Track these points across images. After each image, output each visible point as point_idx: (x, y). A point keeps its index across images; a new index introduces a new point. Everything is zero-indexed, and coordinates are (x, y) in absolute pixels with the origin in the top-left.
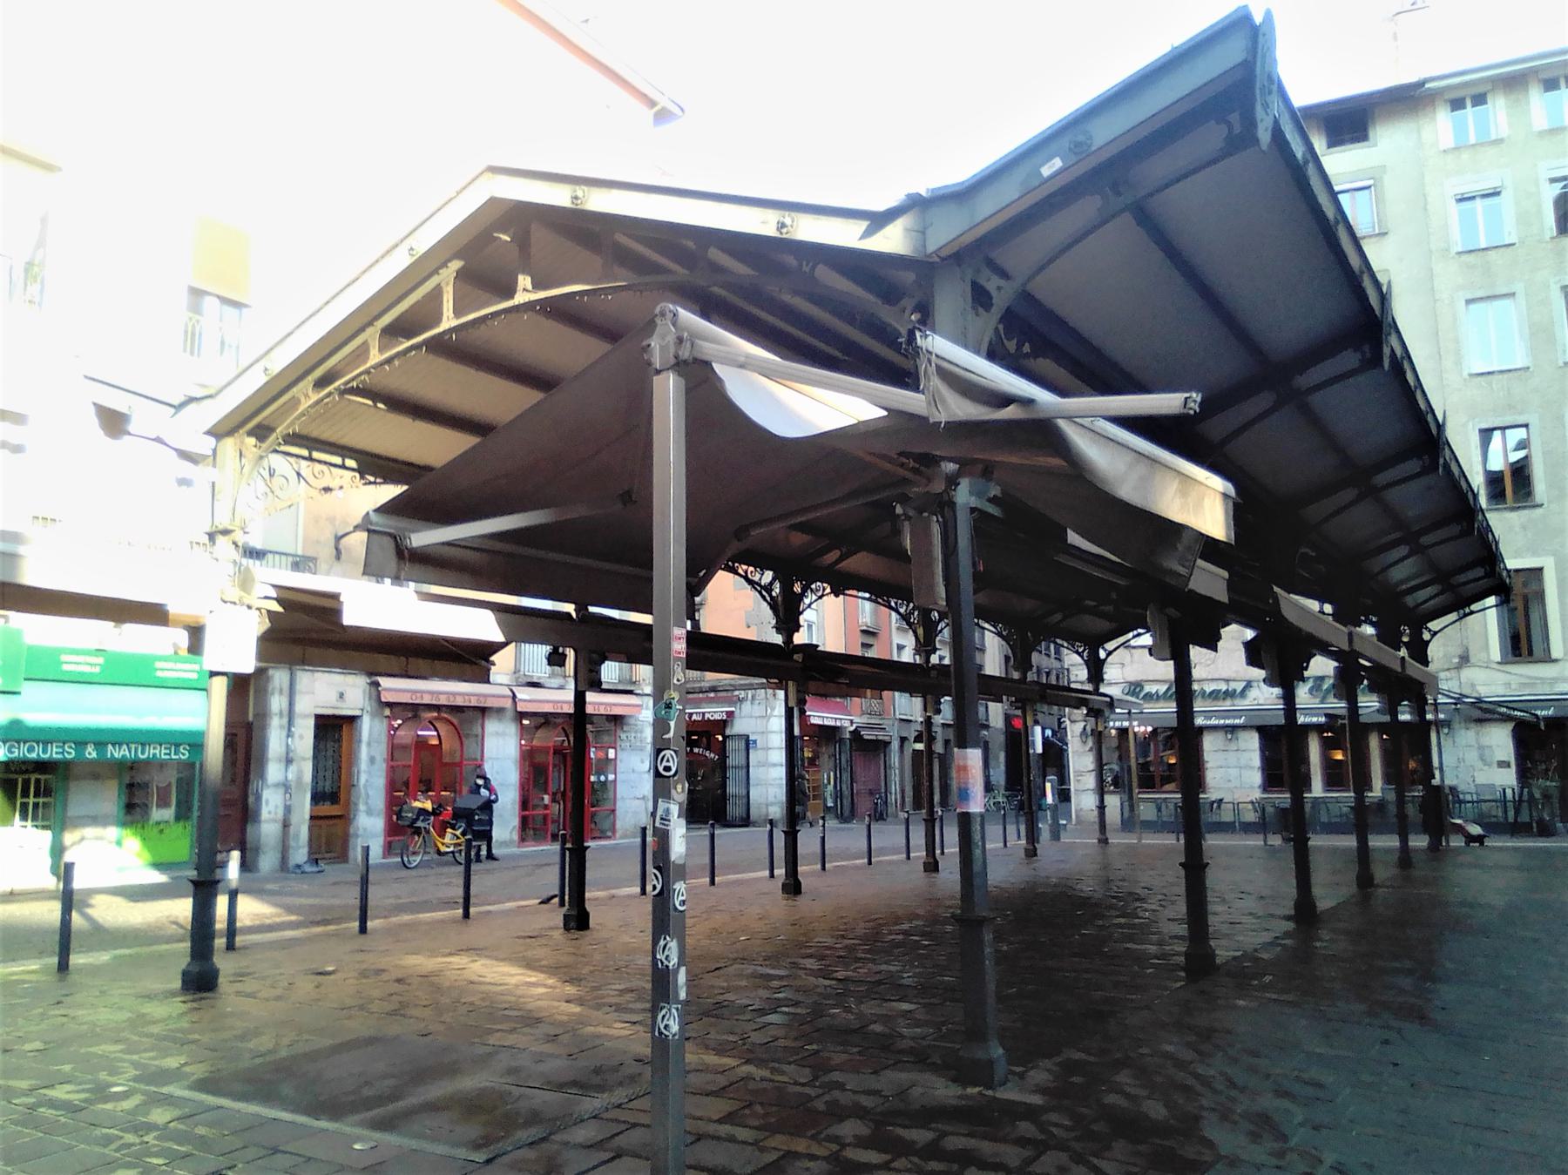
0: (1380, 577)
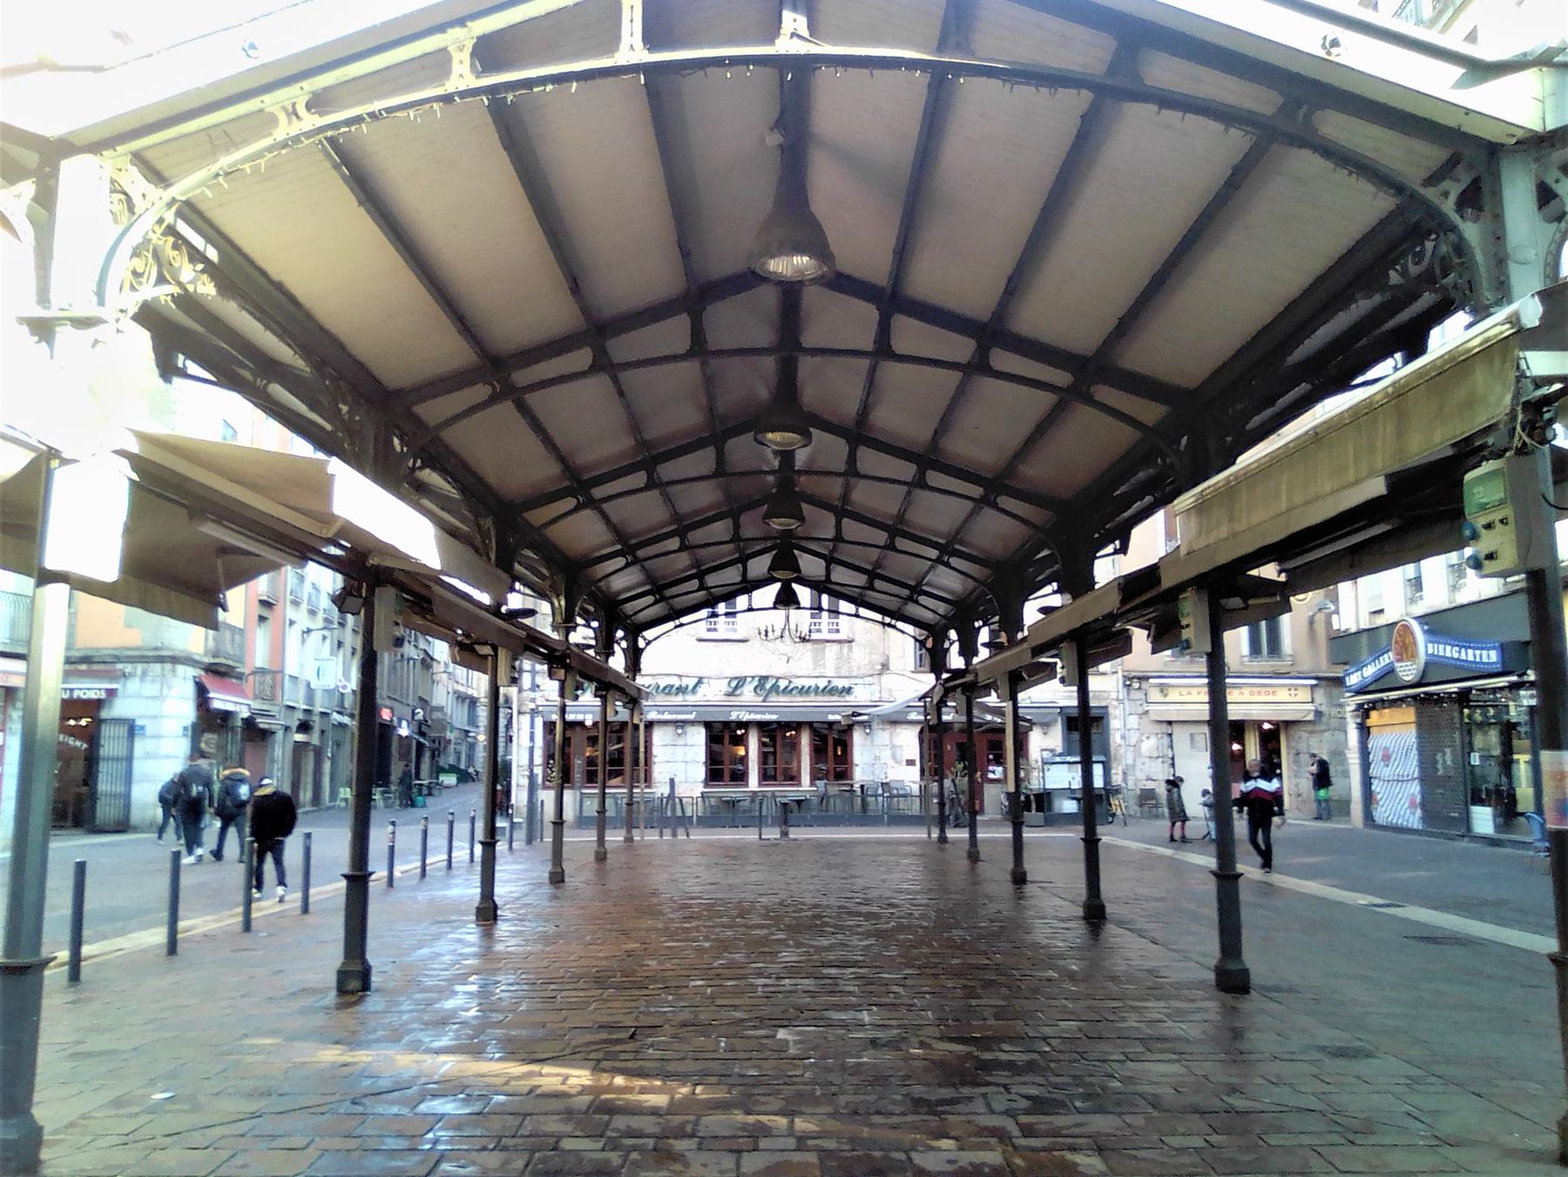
0: (602, 584)
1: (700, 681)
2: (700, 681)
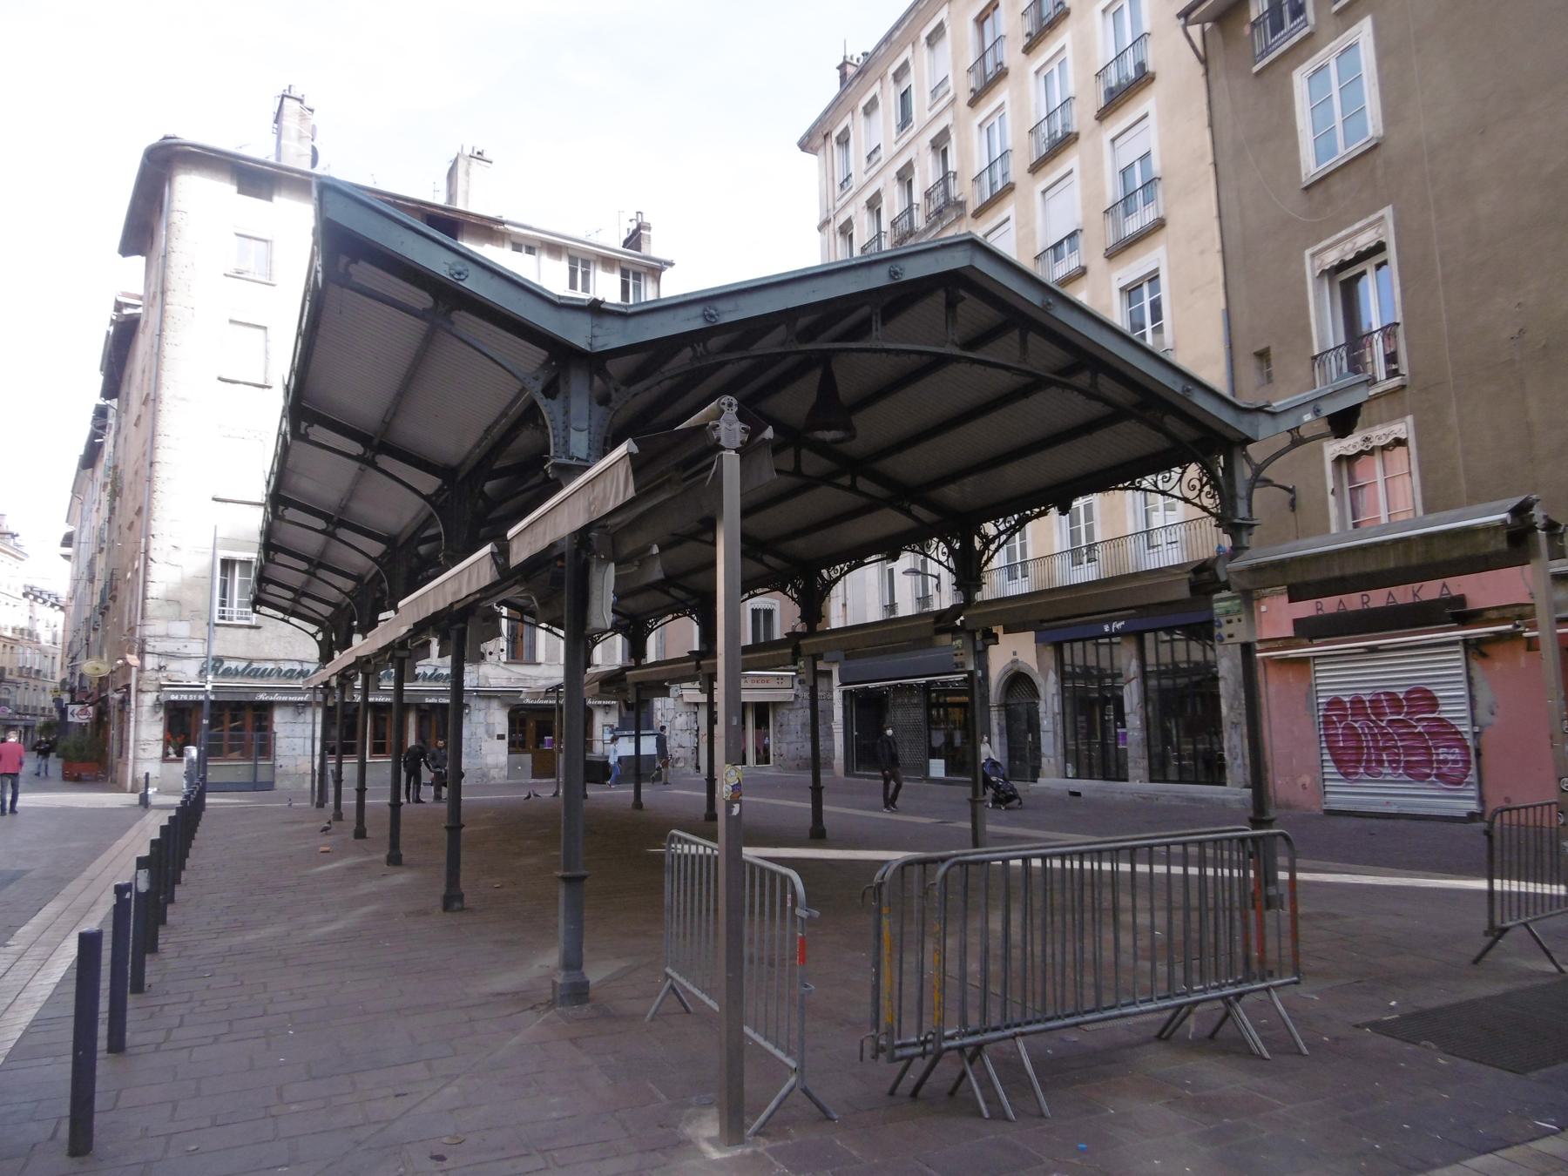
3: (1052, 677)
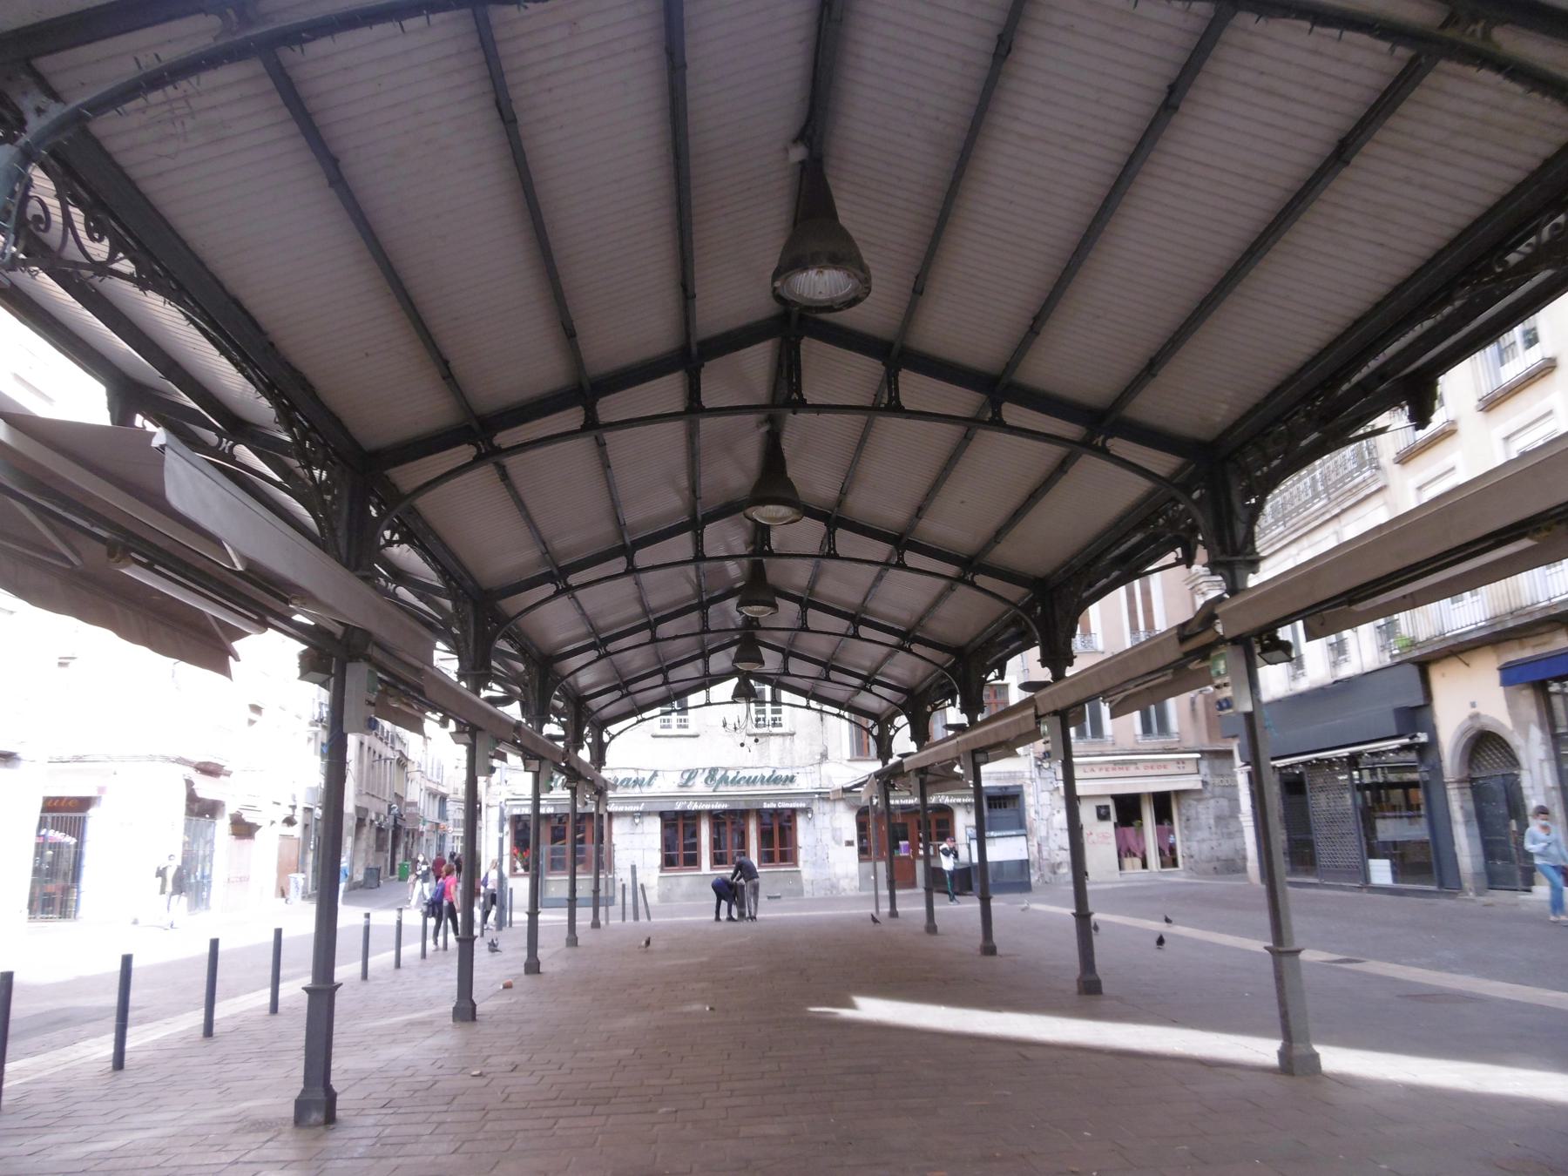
0: (570, 679)
1: (655, 774)
2: (655, 774)
3: (1536, 734)
